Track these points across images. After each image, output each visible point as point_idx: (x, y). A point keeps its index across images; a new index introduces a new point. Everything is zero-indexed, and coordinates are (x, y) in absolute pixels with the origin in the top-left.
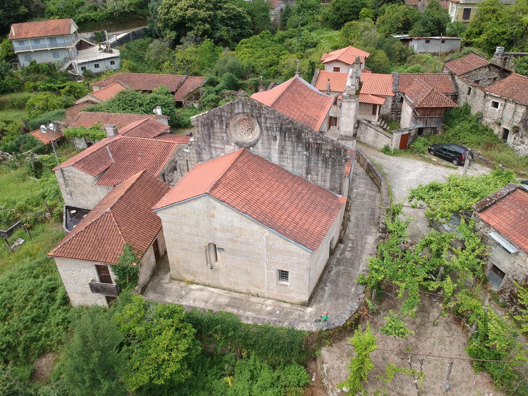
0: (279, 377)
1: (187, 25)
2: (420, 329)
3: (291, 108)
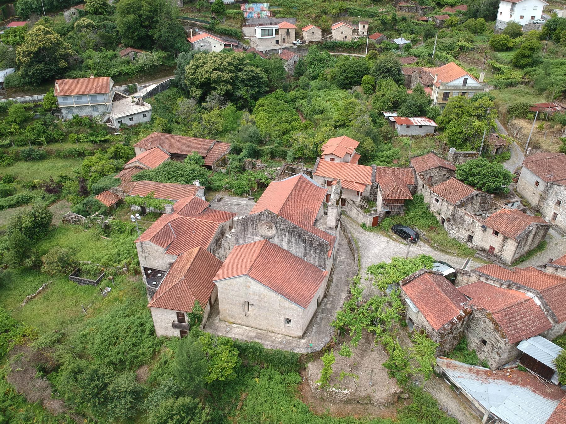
0: (284, 379)
1: (212, 85)
2: (363, 354)
3: (297, 204)
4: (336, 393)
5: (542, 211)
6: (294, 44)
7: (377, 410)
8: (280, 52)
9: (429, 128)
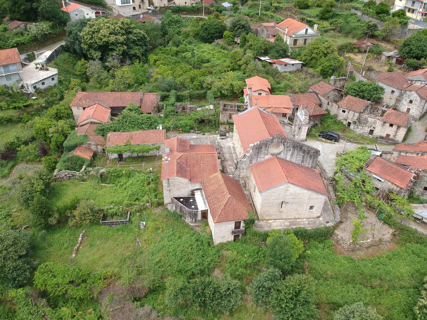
4: (363, 243)
5: (398, 108)
6: (149, 9)
7: (385, 246)
8: (141, 16)
9: (298, 65)
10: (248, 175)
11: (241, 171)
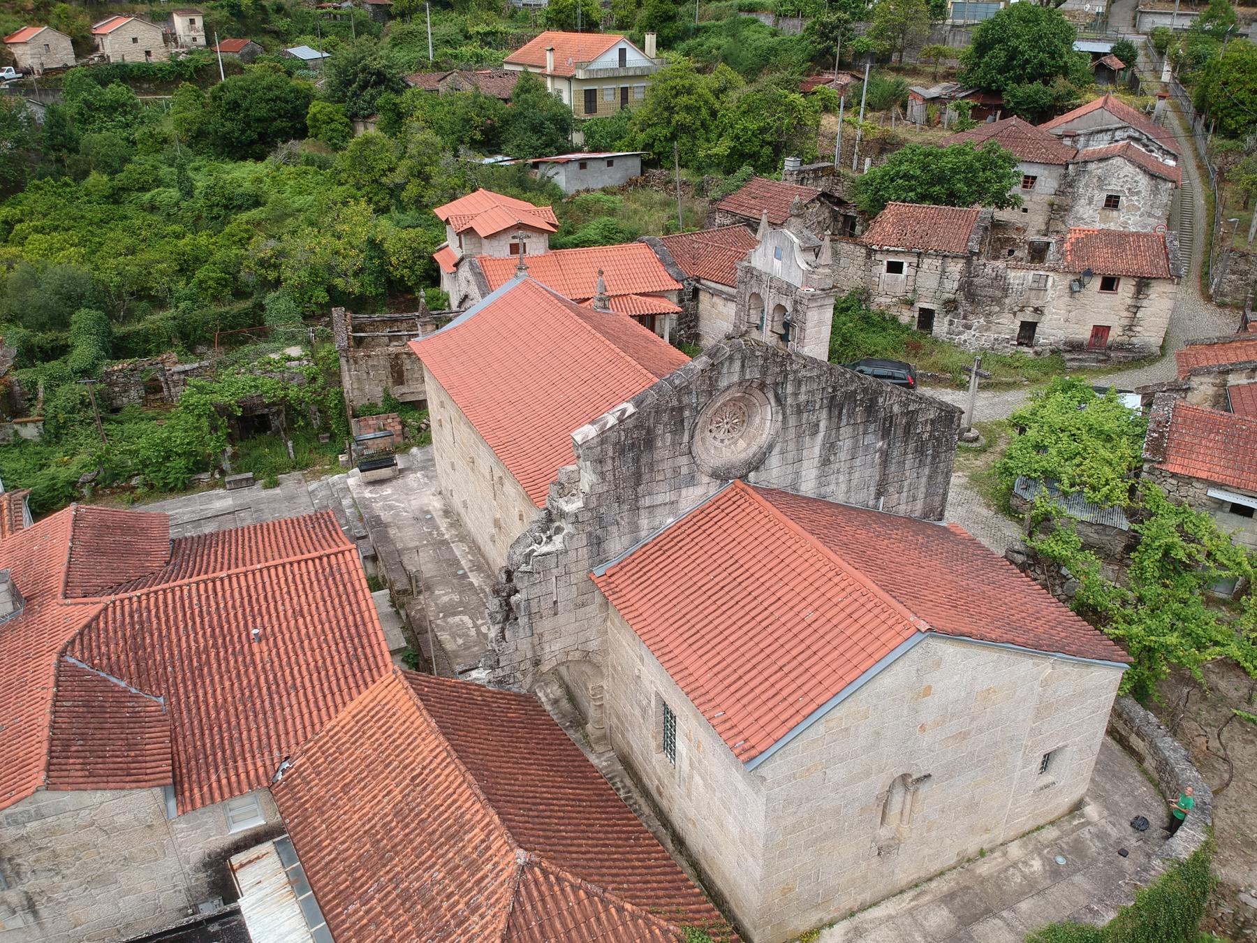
10: (593, 646)
11: (545, 625)
